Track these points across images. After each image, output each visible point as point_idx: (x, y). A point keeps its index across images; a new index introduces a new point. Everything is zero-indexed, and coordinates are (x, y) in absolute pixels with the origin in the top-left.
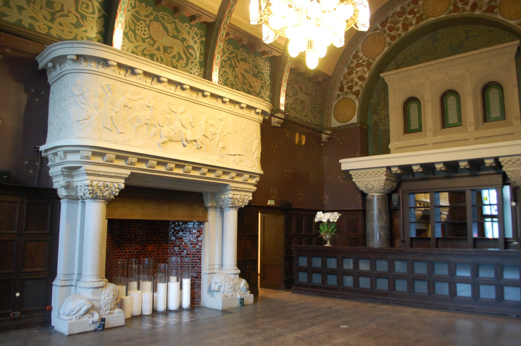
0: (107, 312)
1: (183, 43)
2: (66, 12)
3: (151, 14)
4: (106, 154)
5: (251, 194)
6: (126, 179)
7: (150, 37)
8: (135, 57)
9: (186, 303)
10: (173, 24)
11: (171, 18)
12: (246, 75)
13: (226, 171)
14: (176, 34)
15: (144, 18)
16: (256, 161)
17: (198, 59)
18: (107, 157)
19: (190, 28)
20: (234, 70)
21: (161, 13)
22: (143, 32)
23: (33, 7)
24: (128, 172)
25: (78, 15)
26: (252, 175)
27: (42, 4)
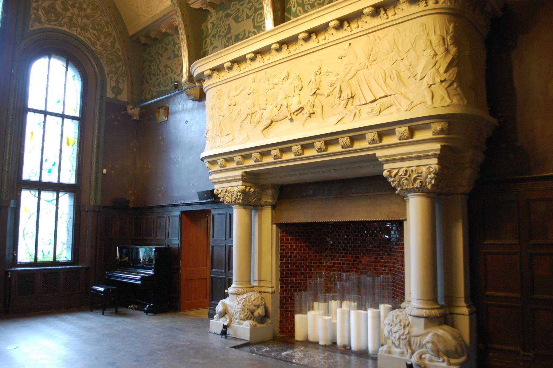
0: (237, 321)
4: (338, 139)
8: (232, 48)
13: (356, 135)
16: (425, 93)
24: (239, 173)
26: (413, 126)
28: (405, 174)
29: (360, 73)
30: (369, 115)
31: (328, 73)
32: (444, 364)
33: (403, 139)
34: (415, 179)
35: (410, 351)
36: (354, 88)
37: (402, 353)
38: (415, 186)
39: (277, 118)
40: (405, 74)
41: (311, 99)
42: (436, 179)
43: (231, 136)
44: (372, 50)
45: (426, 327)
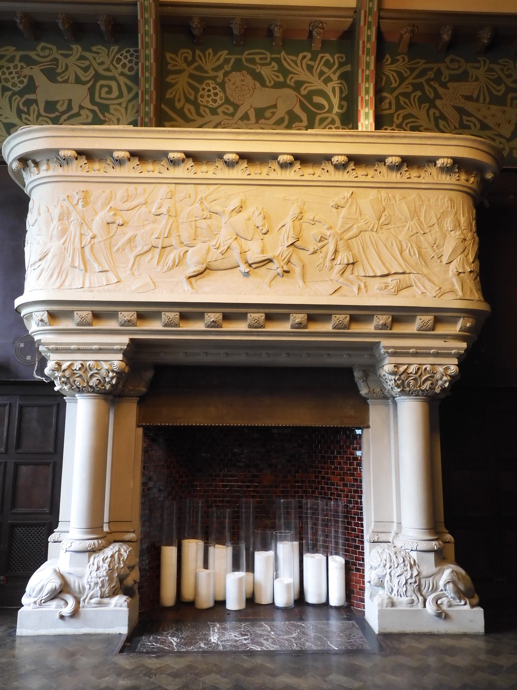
0: (94, 600)
1: (299, 92)
2: (75, 110)
3: (227, 61)
4: (73, 311)
5: (456, 361)
6: (125, 353)
7: (227, 101)
8: (213, 132)
9: (336, 598)
10: (274, 64)
11: (269, 55)
12: (469, 106)
13: (359, 314)
14: (281, 79)
15: (212, 74)
17: (336, 109)
19: (313, 59)
20: (433, 105)
21: (247, 52)
23: (26, 119)
24: (125, 340)
25: (96, 108)
26: (441, 316)
27: (39, 111)
28: (416, 373)
29: (366, 236)
30: (383, 292)
31: (314, 222)
32: (468, 607)
33: (422, 330)
34: (92, 376)
35: (421, 598)
36: (356, 252)
37: (412, 602)
38: (423, 387)
39: (214, 265)
40: (429, 252)
43: (110, 275)
45: (437, 564)
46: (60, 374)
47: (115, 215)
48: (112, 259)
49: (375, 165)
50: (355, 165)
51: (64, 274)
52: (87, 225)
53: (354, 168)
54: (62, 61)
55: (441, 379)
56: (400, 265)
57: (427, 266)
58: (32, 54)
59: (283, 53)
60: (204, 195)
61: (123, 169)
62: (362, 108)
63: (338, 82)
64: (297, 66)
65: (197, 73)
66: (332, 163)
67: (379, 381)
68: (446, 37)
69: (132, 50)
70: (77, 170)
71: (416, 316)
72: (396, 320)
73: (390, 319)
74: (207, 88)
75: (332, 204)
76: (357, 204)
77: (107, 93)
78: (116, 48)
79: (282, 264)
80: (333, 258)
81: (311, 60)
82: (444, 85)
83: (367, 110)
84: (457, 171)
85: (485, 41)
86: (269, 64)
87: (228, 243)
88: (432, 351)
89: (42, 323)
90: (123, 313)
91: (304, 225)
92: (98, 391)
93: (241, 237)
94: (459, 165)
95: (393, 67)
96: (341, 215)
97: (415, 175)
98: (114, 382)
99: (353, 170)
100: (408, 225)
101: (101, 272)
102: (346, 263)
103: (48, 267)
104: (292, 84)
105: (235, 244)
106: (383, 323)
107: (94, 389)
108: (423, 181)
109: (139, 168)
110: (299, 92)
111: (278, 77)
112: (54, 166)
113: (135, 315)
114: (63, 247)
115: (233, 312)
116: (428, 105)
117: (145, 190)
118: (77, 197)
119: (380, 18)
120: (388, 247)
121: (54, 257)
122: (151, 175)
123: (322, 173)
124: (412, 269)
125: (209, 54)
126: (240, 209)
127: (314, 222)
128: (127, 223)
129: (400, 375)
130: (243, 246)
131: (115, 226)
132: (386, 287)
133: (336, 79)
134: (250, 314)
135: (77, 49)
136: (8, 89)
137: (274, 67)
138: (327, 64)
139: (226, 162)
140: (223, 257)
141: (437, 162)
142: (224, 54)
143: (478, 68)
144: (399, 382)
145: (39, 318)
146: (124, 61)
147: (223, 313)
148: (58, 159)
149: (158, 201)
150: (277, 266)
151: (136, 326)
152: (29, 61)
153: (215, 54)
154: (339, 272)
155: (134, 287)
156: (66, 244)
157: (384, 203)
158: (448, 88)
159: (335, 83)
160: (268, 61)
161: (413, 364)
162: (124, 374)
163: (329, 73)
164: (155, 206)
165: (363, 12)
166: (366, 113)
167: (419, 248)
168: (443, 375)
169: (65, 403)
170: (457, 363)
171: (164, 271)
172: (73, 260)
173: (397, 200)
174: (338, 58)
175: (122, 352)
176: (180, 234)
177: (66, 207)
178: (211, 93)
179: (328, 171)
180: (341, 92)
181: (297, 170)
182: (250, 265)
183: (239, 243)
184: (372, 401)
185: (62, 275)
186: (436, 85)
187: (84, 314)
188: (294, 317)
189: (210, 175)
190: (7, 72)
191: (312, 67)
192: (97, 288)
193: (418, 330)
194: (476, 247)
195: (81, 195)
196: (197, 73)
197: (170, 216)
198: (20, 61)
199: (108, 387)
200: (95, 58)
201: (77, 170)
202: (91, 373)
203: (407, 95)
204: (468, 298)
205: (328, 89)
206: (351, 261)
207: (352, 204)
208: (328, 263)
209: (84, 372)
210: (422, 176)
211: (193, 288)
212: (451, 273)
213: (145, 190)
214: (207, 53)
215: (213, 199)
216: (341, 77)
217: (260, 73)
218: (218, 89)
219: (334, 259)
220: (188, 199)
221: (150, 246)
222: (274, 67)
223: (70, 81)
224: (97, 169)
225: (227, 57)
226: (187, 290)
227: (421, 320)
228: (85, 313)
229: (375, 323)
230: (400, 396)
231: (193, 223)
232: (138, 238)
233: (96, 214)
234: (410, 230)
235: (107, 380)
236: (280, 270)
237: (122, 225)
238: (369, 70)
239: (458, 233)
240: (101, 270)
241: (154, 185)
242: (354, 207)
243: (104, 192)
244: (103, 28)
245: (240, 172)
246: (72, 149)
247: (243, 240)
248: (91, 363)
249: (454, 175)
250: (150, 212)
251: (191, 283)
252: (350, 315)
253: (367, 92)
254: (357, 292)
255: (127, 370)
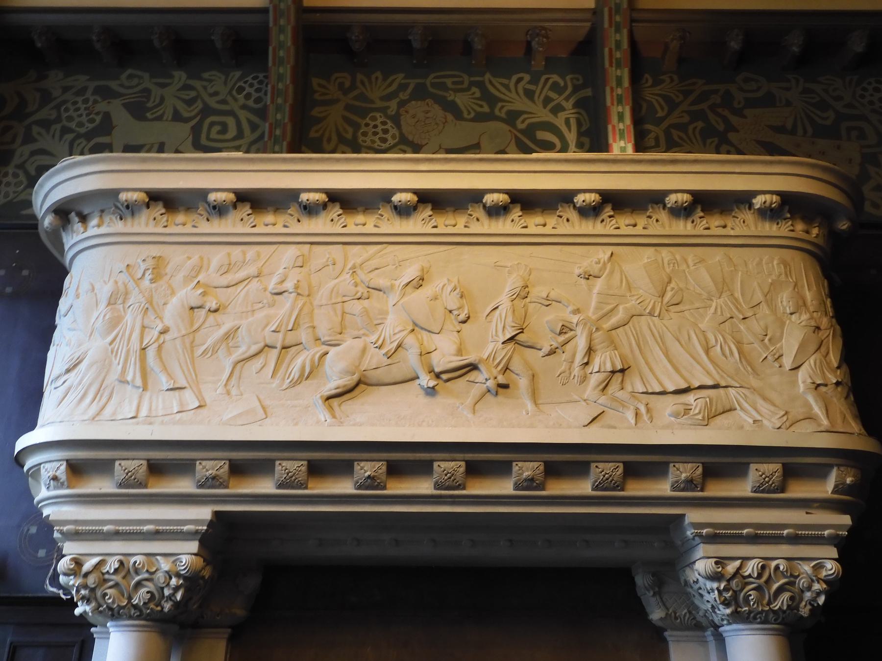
1: (513, 125)
3: (403, 87)
4: (114, 460)
5: (833, 552)
10: (474, 89)
11: (466, 79)
14: (486, 109)
15: (379, 104)
18: (120, 470)
19: (534, 81)
21: (432, 75)
22: (381, 135)
24: (205, 513)
26: (796, 463)
28: (760, 576)
31: (548, 302)
33: (763, 492)
34: (139, 585)
36: (626, 351)
38: (776, 606)
39: (374, 376)
40: (758, 351)
41: (503, 353)
42: (829, 594)
43: (188, 395)
44: (670, 282)
46: (79, 581)
47: (204, 294)
48: (195, 371)
49: (647, 210)
50: (613, 209)
51: (106, 394)
52: (155, 311)
53: (612, 213)
54: (156, 92)
55: (809, 588)
56: (708, 373)
57: (758, 375)
58: (113, 85)
59: (488, 76)
60: (359, 261)
61: (223, 221)
62: (615, 141)
63: (573, 111)
64: (510, 91)
65: (357, 103)
66: (574, 206)
67: (686, 593)
68: (735, 45)
69: (261, 76)
70: (147, 224)
71: (749, 464)
72: (711, 473)
73: (700, 470)
74: (372, 123)
75: (577, 271)
76: (622, 272)
77: (219, 133)
78: (238, 74)
79: (495, 372)
80: (586, 361)
81: (529, 83)
82: (739, 113)
83: (622, 144)
84: (789, 215)
85: (795, 49)
86: (468, 89)
87: (399, 336)
88: (785, 532)
89: (55, 483)
90: (204, 463)
91: (531, 307)
92: (148, 614)
93: (422, 328)
94: (790, 205)
95: (657, 90)
96: (596, 291)
97: (717, 223)
98: (179, 596)
99: (610, 217)
100: (714, 304)
101: (171, 389)
102: (609, 368)
103: (80, 383)
104: (503, 115)
105: (410, 340)
106: (687, 477)
107: (141, 611)
108: (732, 233)
109: (252, 220)
110: (513, 125)
111: (481, 106)
112: (111, 219)
113: (226, 467)
114: (110, 348)
115: (406, 458)
116: (716, 140)
117: (259, 255)
118: (143, 267)
119: (633, 21)
120: (683, 343)
121: (91, 366)
122: (270, 230)
123: (558, 224)
124: (729, 379)
125: (377, 78)
126: (419, 282)
127: (548, 302)
128: (225, 307)
129: (728, 581)
130: (425, 343)
131: (203, 312)
132: (687, 411)
133: (570, 107)
134: (439, 463)
135: (180, 77)
136: (70, 131)
137: (474, 93)
138: (555, 87)
139: (396, 207)
140: (390, 361)
141: (754, 201)
142: (399, 78)
143: (788, 89)
144: (728, 595)
145: (51, 474)
146: (248, 90)
147: (387, 461)
148: (117, 207)
149: (281, 271)
150: (487, 376)
151: (227, 487)
152: (107, 94)
153: (385, 79)
154: (598, 386)
155: (227, 416)
156: (116, 345)
157: (668, 270)
158: (745, 117)
159: (569, 112)
160: (466, 85)
161: (751, 559)
162: (201, 582)
163: (558, 99)
164: (275, 280)
165: (606, 10)
166: (621, 148)
167: (739, 344)
168: (813, 581)
169: (93, 640)
170: (837, 556)
171: (284, 387)
172: (124, 371)
173: (691, 263)
174: (572, 79)
175: (199, 537)
176: (315, 324)
177: (124, 283)
178: (379, 129)
179: (568, 220)
180: (579, 124)
181: (517, 219)
182: (438, 376)
183: (418, 339)
184: (675, 633)
185: (101, 397)
186: (726, 113)
187: (131, 465)
188: (521, 468)
189: (370, 228)
190: (72, 108)
191: (534, 92)
192: (160, 419)
193: (755, 492)
194: (840, 342)
195: (150, 263)
196: (357, 103)
197: (299, 294)
198: (93, 94)
199: (167, 606)
200: (205, 88)
201: (147, 224)
202: (137, 578)
203: (682, 127)
204: (841, 430)
205: (559, 121)
206: (619, 367)
207: (612, 272)
208: (576, 370)
209: (124, 578)
210: (729, 225)
211: (334, 417)
212: (802, 386)
213: (259, 255)
214: (373, 77)
215: (374, 267)
216: (576, 105)
217: (453, 103)
218: (390, 124)
219: (587, 364)
220: (331, 267)
221: (262, 345)
222: (474, 93)
223: (165, 118)
224: (182, 224)
225: (403, 81)
226: (323, 419)
227: (761, 471)
228: (132, 464)
229: (671, 478)
230: (729, 624)
231: (339, 306)
232: (242, 332)
233: (173, 293)
234: (719, 313)
235: (167, 592)
236: (491, 384)
237: (216, 311)
238: (621, 88)
239: (805, 317)
240: (171, 387)
241: (275, 247)
242: (617, 276)
243: (189, 258)
244: (219, 45)
245: (420, 223)
246: (140, 190)
247: (424, 333)
248: (138, 559)
249: (784, 222)
250: (265, 290)
251: (331, 408)
252: (624, 463)
253: (621, 118)
254: (633, 422)
255: (207, 573)
